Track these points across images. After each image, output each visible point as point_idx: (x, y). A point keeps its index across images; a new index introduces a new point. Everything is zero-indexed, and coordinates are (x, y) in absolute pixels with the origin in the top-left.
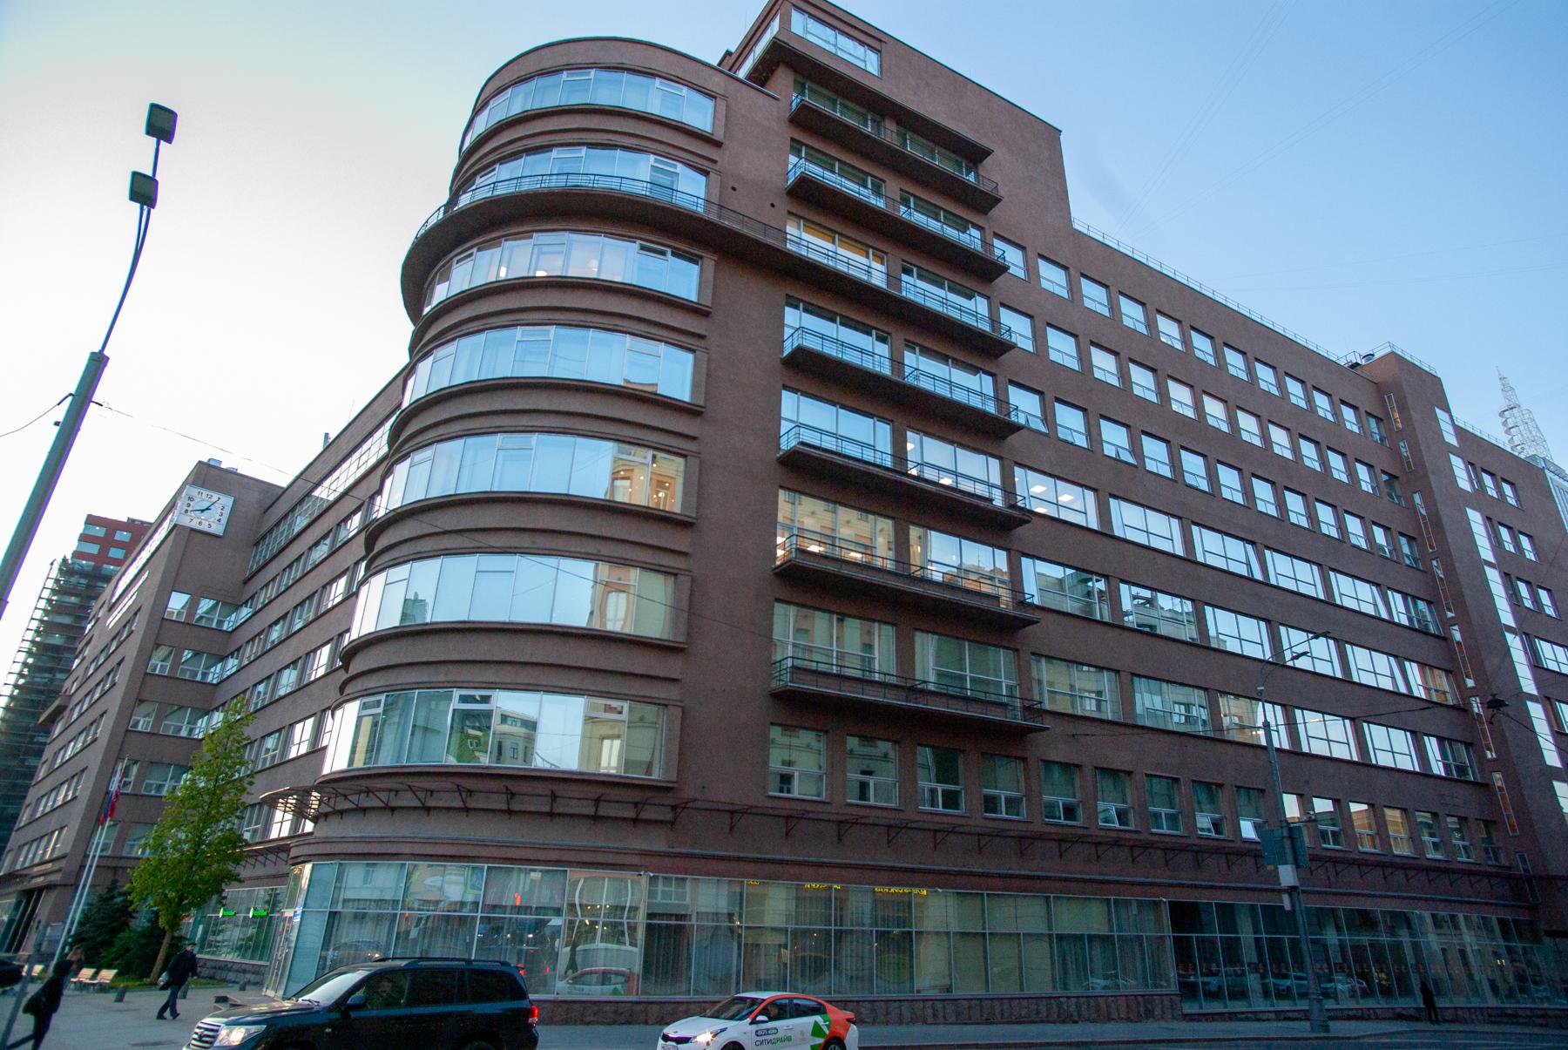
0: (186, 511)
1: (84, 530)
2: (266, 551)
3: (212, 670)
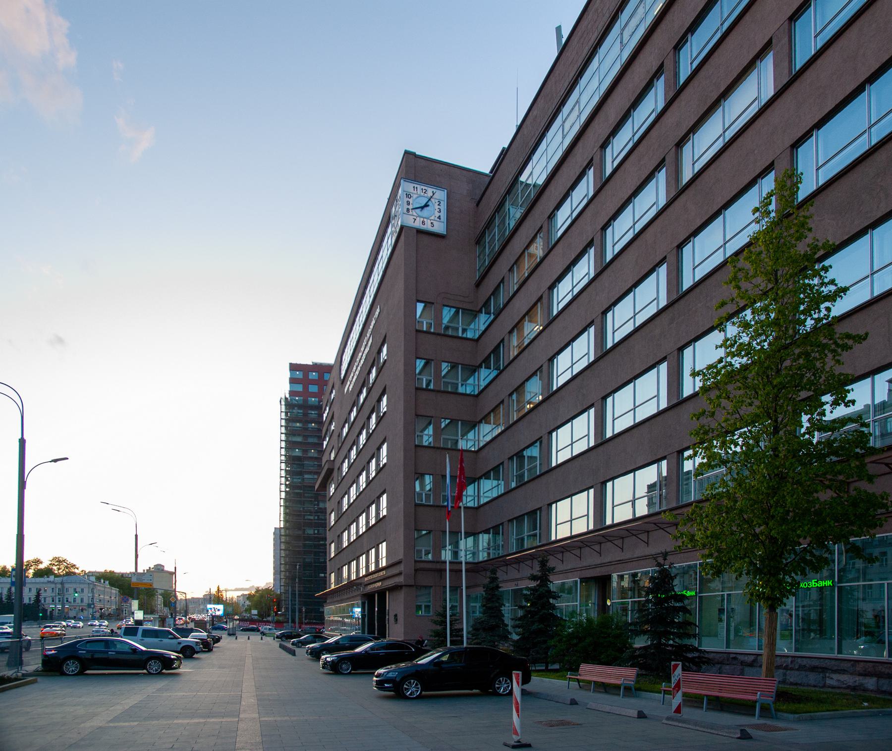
0: (408, 210)
2: (496, 236)
3: (426, 432)
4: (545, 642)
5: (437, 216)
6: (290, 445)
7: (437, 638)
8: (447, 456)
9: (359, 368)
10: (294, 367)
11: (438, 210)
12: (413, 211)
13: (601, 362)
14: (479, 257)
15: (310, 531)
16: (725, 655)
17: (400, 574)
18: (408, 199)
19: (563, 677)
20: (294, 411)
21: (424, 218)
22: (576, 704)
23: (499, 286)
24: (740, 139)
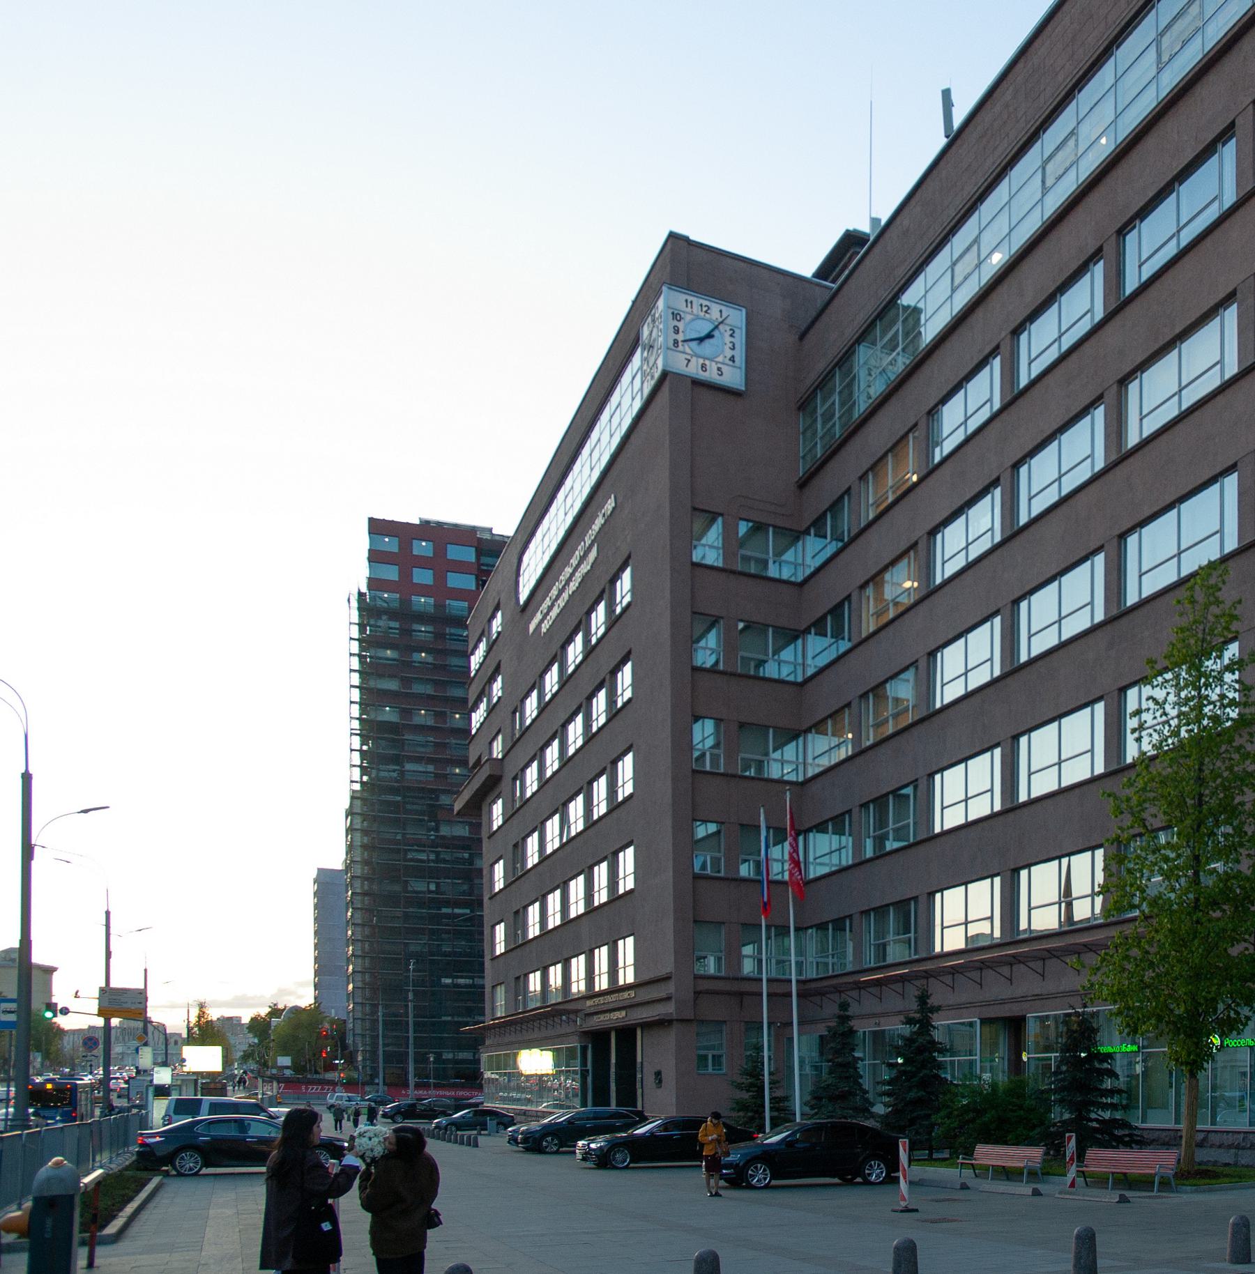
0: (676, 342)
1: (371, 545)
4: (928, 1116)
5: (729, 356)
6: (370, 698)
7: (741, 1114)
8: (762, 810)
9: (565, 596)
10: (377, 527)
11: (731, 345)
12: (685, 344)
13: (1009, 680)
14: (804, 433)
15: (419, 886)
16: (1172, 1134)
17: (668, 999)
18: (676, 323)
19: (954, 1165)
20: (381, 623)
21: (705, 358)
22: (968, 1188)
23: (841, 498)
24: (1197, 414)
